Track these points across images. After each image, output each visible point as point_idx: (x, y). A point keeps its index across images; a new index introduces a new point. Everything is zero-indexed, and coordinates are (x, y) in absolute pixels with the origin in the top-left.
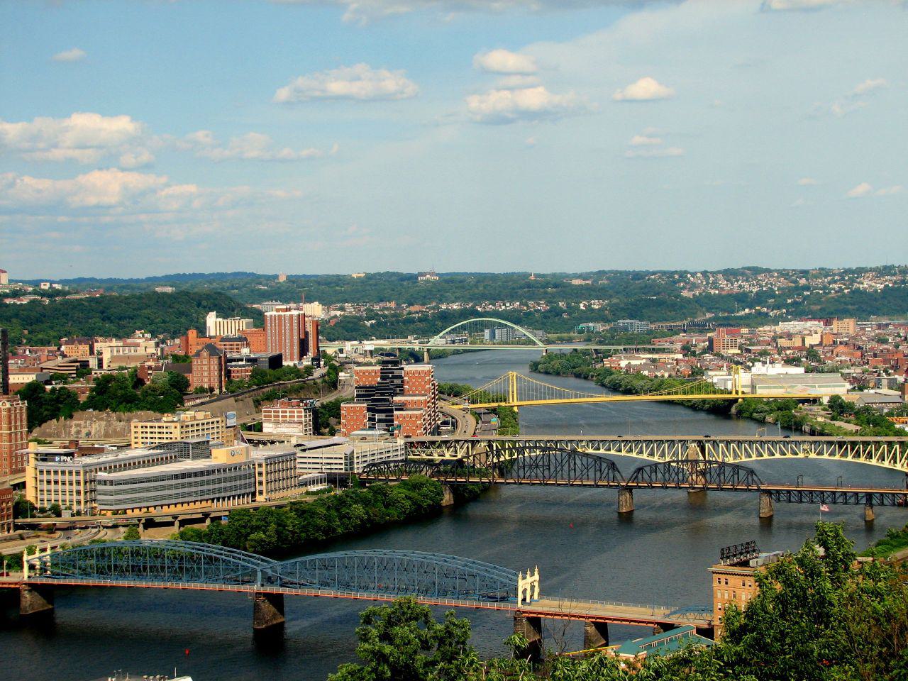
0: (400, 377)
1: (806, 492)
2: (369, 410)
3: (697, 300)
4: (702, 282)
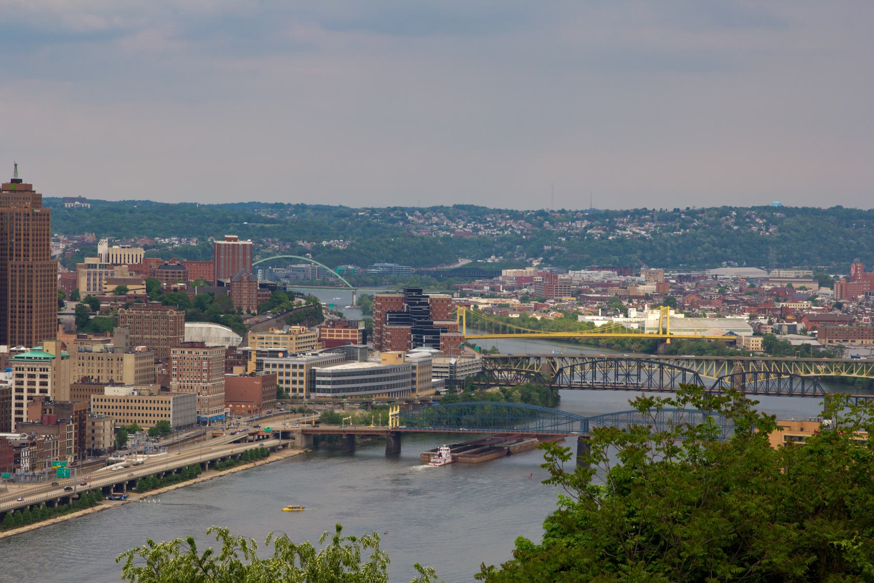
0: (426, 304)
2: (413, 332)
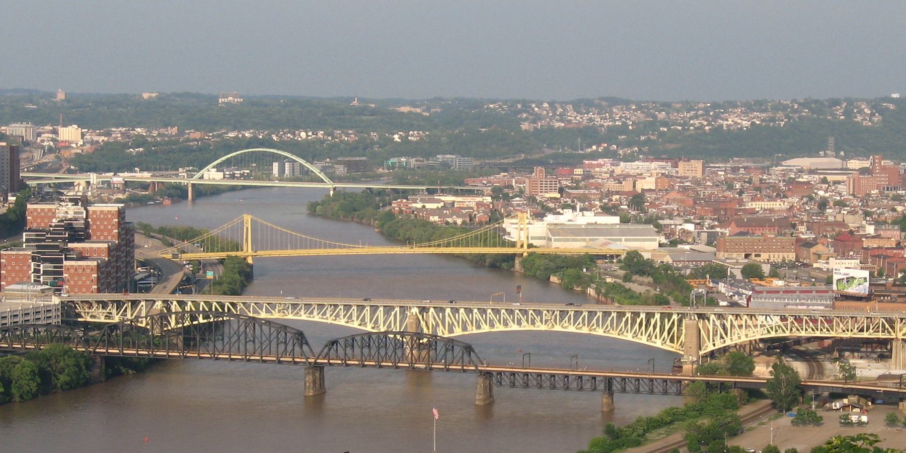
1: (546, 375)
2: (34, 259)
3: (537, 133)
4: (548, 113)
